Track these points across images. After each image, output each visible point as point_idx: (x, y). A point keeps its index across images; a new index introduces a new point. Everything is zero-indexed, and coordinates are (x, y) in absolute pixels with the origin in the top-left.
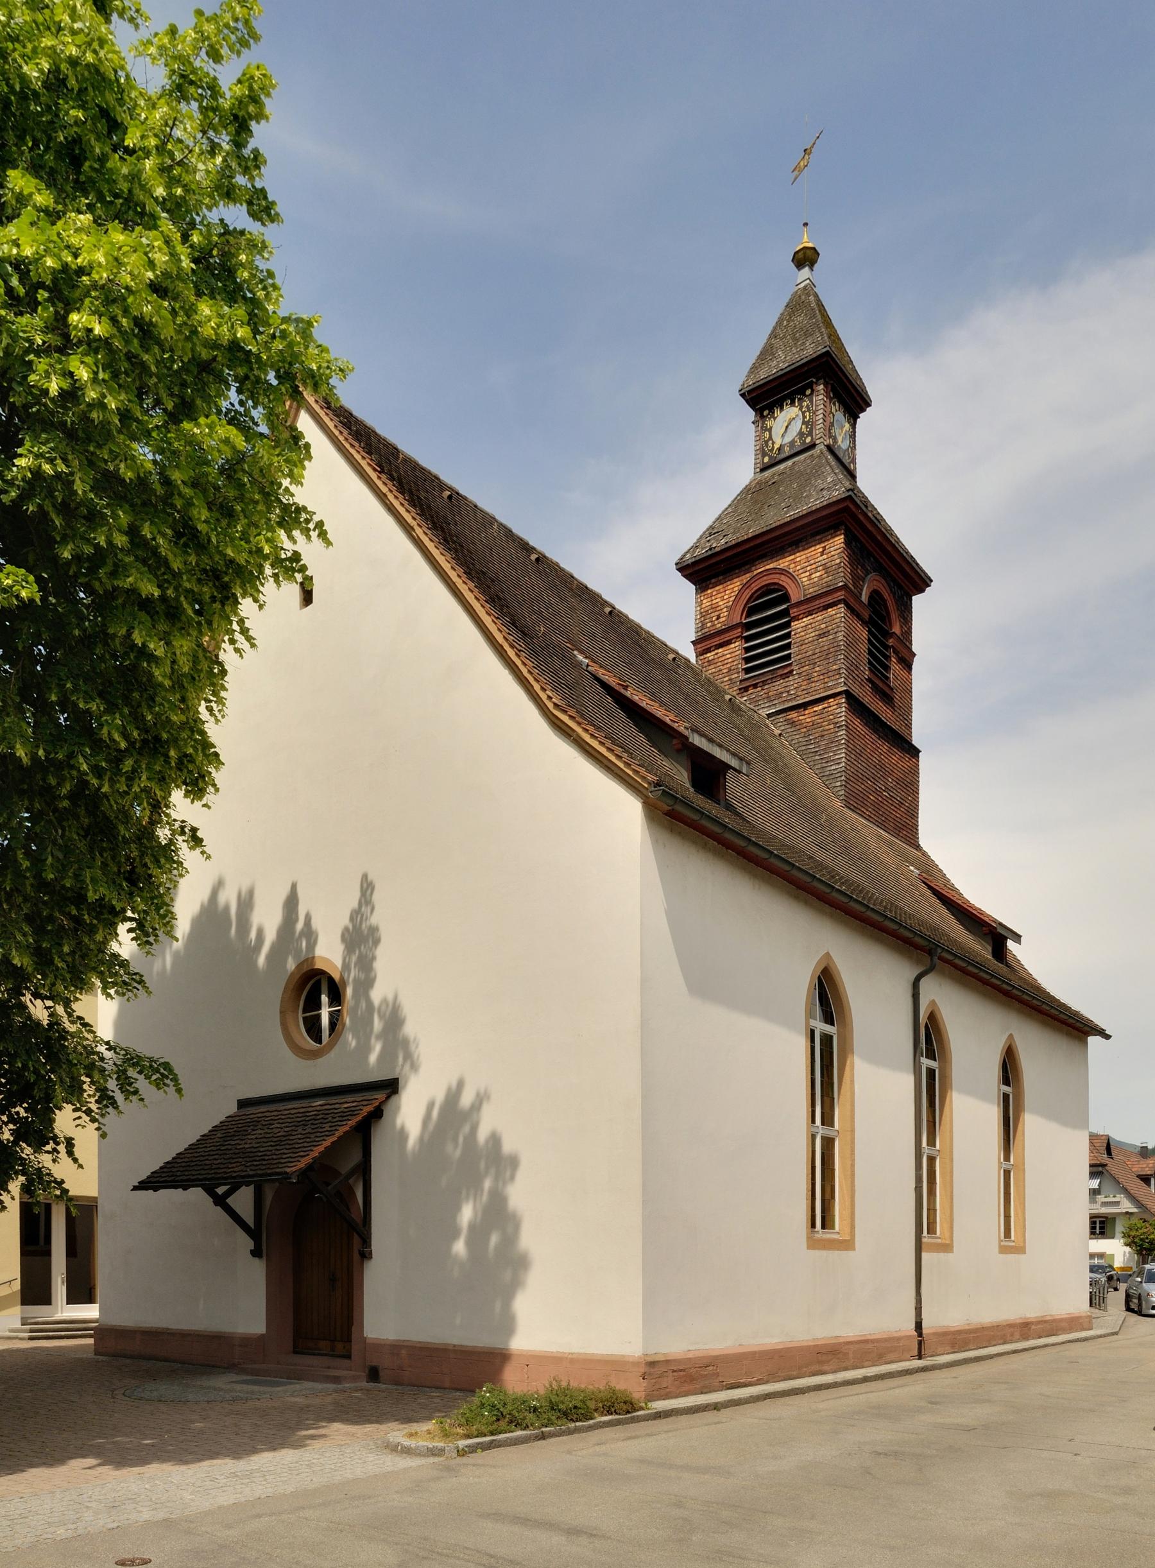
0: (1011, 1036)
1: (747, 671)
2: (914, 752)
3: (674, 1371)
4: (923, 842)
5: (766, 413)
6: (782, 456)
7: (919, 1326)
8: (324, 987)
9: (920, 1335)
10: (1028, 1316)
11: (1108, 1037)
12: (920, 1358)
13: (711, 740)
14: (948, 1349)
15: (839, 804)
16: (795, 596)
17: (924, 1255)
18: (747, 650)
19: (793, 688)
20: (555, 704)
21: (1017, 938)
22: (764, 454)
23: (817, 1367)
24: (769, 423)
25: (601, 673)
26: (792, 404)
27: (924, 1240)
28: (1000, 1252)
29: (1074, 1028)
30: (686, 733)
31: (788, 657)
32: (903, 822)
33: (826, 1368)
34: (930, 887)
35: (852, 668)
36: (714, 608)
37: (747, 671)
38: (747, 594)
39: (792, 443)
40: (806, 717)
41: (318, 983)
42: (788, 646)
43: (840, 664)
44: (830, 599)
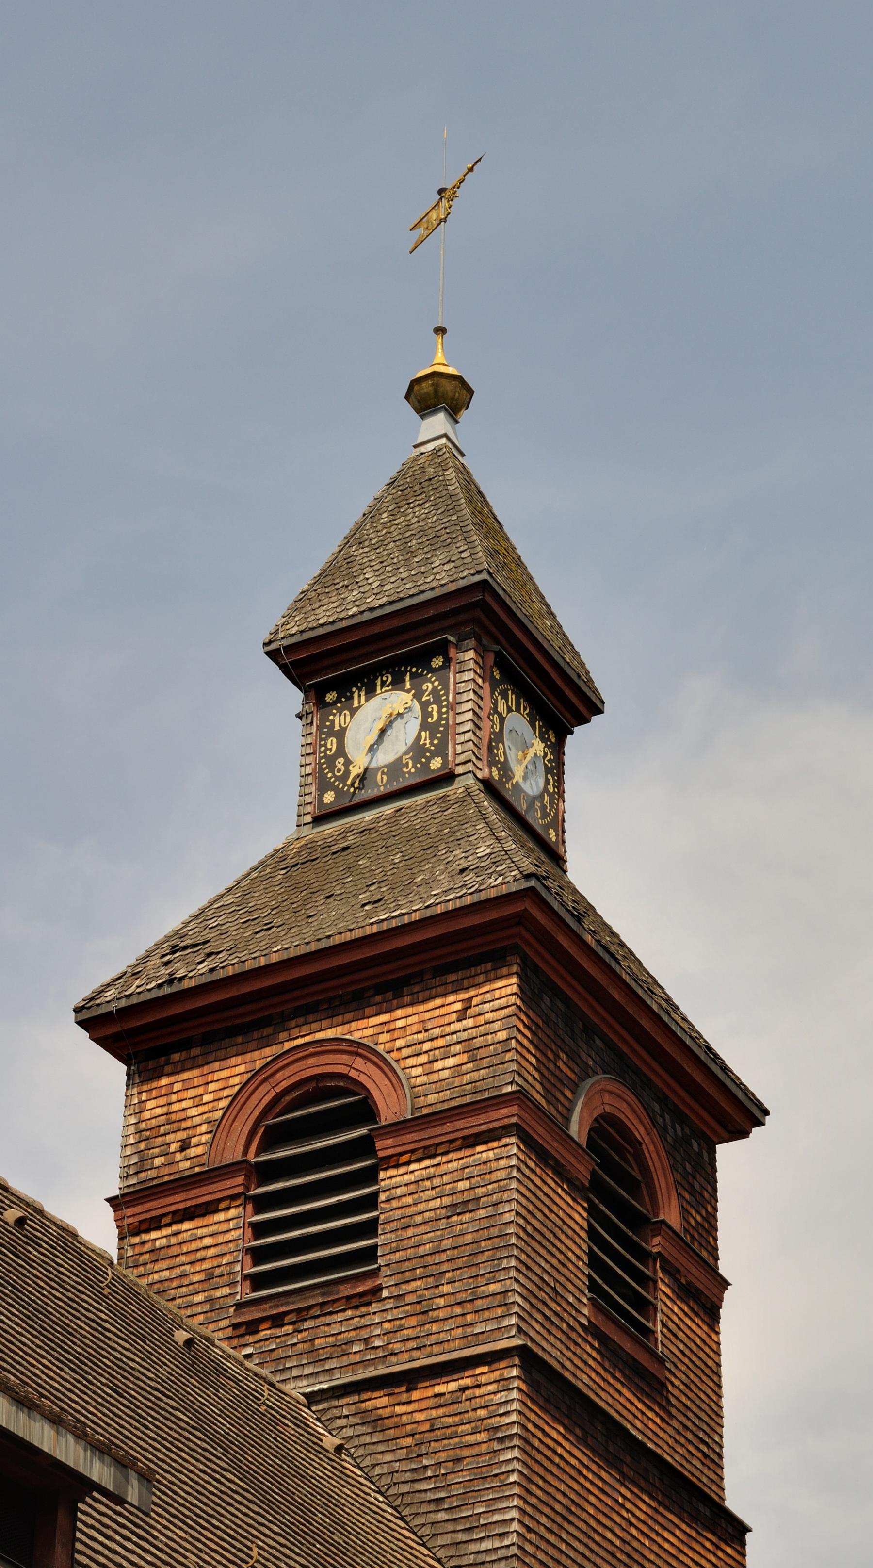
2: (734, 1531)
5: (330, 697)
6: (369, 793)
16: (390, 1107)
18: (259, 1230)
19: (381, 1334)
22: (324, 786)
24: (338, 720)
26: (397, 683)
31: (370, 1254)
35: (541, 1297)
36: (174, 1122)
38: (264, 1095)
39: (395, 768)
40: (416, 1407)
43: (507, 1281)
44: (480, 1123)
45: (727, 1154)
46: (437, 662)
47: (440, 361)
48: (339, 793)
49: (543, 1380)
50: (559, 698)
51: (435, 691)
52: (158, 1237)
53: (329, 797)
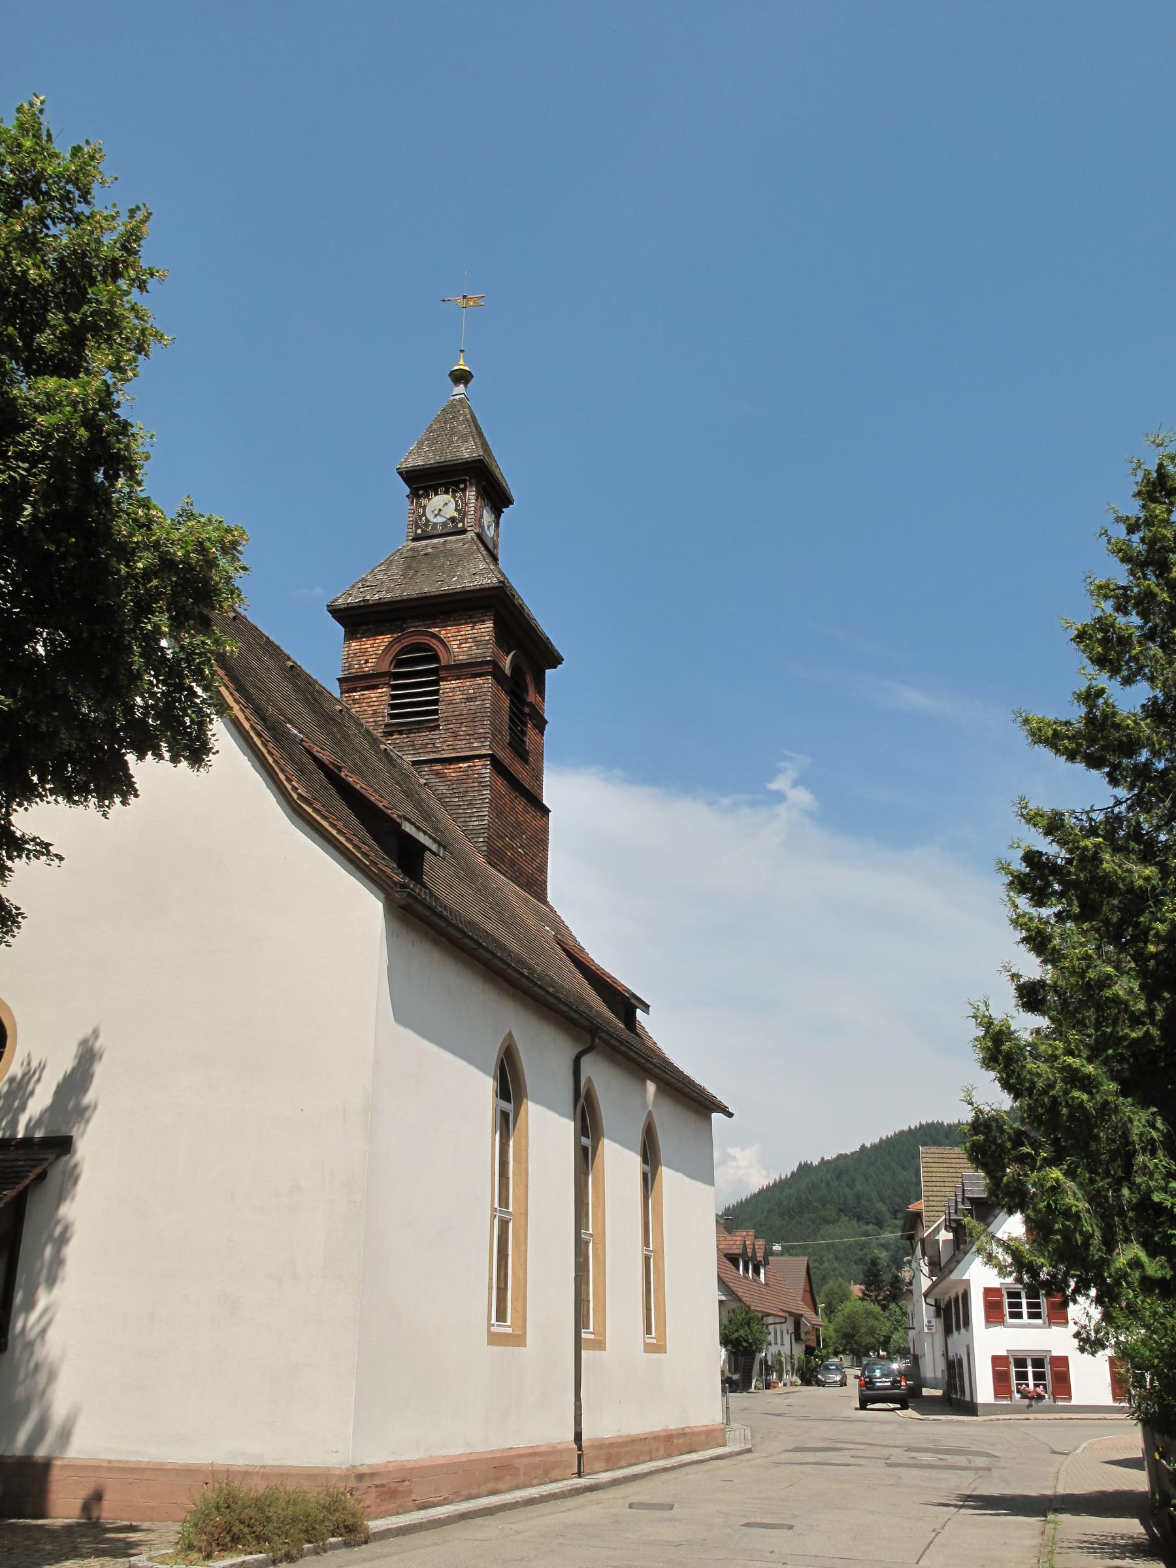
0: (510, 1035)
1: (393, 716)
2: (545, 811)
3: (377, 1486)
5: (421, 492)
6: (435, 532)
7: (578, 1437)
9: (580, 1448)
10: (671, 1427)
11: (730, 1115)
12: (580, 1477)
13: (419, 829)
14: (603, 1466)
15: (481, 860)
16: (444, 660)
17: (584, 1353)
18: (394, 697)
19: (442, 743)
20: (300, 795)
21: (646, 1007)
22: (417, 527)
23: (491, 1486)
24: (424, 502)
25: (315, 750)
26: (447, 492)
27: (583, 1336)
28: (645, 1351)
29: (699, 1104)
30: (399, 820)
31: (435, 712)
32: (534, 883)
33: (501, 1486)
34: (564, 949)
35: (496, 732)
37: (393, 716)
38: (397, 648)
39: (444, 524)
40: (451, 771)
42: (436, 702)
43: (485, 727)
44: (479, 670)
46: (462, 486)
47: (462, 365)
49: (497, 765)
50: (497, 497)
52: (356, 695)
53: (419, 531)
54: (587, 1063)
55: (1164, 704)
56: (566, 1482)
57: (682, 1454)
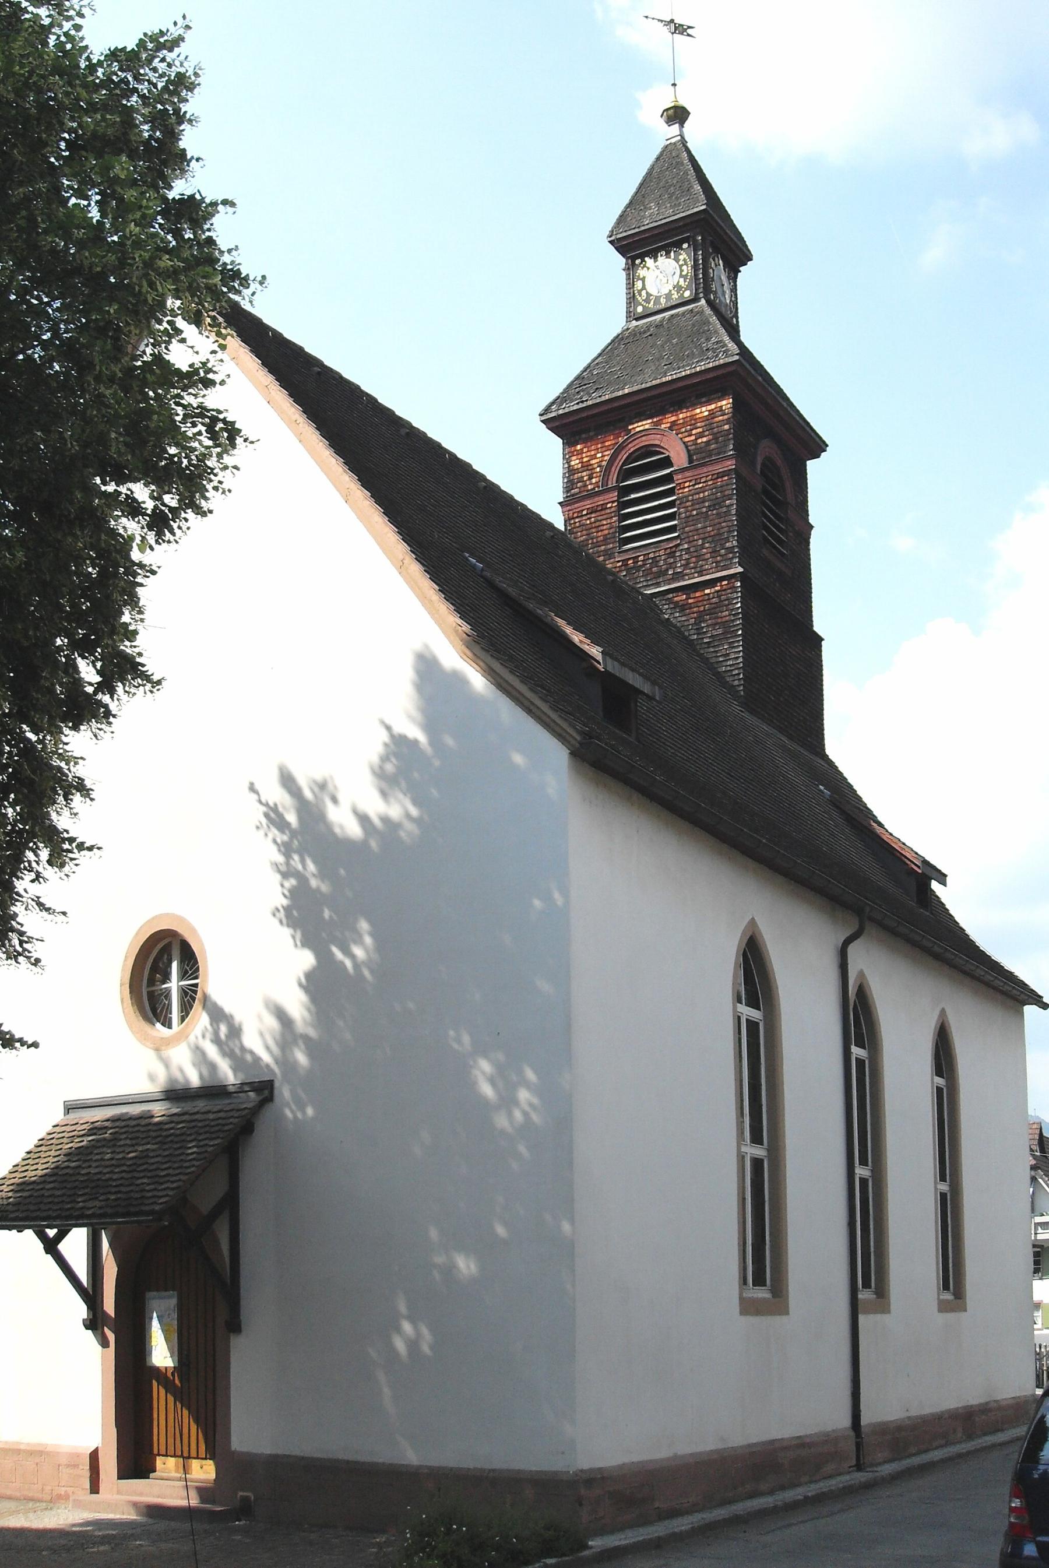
0: (943, 1012)
4: (828, 751)
5: (638, 261)
8: (176, 952)
17: (862, 1318)
21: (942, 878)
25: (498, 580)
27: (860, 1296)
28: (940, 1310)
29: (1010, 993)
33: (763, 1487)
36: (586, 466)
39: (668, 296)
41: (169, 945)
45: (811, 465)
48: (644, 307)
51: (684, 260)
54: (860, 958)
55: (288, 864)
56: (839, 1478)
57: (985, 1434)
